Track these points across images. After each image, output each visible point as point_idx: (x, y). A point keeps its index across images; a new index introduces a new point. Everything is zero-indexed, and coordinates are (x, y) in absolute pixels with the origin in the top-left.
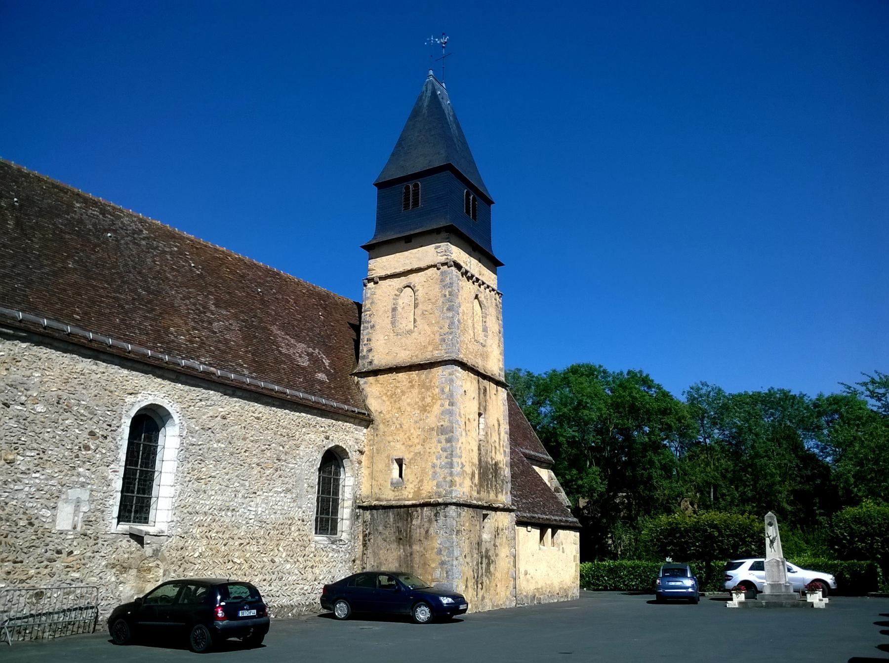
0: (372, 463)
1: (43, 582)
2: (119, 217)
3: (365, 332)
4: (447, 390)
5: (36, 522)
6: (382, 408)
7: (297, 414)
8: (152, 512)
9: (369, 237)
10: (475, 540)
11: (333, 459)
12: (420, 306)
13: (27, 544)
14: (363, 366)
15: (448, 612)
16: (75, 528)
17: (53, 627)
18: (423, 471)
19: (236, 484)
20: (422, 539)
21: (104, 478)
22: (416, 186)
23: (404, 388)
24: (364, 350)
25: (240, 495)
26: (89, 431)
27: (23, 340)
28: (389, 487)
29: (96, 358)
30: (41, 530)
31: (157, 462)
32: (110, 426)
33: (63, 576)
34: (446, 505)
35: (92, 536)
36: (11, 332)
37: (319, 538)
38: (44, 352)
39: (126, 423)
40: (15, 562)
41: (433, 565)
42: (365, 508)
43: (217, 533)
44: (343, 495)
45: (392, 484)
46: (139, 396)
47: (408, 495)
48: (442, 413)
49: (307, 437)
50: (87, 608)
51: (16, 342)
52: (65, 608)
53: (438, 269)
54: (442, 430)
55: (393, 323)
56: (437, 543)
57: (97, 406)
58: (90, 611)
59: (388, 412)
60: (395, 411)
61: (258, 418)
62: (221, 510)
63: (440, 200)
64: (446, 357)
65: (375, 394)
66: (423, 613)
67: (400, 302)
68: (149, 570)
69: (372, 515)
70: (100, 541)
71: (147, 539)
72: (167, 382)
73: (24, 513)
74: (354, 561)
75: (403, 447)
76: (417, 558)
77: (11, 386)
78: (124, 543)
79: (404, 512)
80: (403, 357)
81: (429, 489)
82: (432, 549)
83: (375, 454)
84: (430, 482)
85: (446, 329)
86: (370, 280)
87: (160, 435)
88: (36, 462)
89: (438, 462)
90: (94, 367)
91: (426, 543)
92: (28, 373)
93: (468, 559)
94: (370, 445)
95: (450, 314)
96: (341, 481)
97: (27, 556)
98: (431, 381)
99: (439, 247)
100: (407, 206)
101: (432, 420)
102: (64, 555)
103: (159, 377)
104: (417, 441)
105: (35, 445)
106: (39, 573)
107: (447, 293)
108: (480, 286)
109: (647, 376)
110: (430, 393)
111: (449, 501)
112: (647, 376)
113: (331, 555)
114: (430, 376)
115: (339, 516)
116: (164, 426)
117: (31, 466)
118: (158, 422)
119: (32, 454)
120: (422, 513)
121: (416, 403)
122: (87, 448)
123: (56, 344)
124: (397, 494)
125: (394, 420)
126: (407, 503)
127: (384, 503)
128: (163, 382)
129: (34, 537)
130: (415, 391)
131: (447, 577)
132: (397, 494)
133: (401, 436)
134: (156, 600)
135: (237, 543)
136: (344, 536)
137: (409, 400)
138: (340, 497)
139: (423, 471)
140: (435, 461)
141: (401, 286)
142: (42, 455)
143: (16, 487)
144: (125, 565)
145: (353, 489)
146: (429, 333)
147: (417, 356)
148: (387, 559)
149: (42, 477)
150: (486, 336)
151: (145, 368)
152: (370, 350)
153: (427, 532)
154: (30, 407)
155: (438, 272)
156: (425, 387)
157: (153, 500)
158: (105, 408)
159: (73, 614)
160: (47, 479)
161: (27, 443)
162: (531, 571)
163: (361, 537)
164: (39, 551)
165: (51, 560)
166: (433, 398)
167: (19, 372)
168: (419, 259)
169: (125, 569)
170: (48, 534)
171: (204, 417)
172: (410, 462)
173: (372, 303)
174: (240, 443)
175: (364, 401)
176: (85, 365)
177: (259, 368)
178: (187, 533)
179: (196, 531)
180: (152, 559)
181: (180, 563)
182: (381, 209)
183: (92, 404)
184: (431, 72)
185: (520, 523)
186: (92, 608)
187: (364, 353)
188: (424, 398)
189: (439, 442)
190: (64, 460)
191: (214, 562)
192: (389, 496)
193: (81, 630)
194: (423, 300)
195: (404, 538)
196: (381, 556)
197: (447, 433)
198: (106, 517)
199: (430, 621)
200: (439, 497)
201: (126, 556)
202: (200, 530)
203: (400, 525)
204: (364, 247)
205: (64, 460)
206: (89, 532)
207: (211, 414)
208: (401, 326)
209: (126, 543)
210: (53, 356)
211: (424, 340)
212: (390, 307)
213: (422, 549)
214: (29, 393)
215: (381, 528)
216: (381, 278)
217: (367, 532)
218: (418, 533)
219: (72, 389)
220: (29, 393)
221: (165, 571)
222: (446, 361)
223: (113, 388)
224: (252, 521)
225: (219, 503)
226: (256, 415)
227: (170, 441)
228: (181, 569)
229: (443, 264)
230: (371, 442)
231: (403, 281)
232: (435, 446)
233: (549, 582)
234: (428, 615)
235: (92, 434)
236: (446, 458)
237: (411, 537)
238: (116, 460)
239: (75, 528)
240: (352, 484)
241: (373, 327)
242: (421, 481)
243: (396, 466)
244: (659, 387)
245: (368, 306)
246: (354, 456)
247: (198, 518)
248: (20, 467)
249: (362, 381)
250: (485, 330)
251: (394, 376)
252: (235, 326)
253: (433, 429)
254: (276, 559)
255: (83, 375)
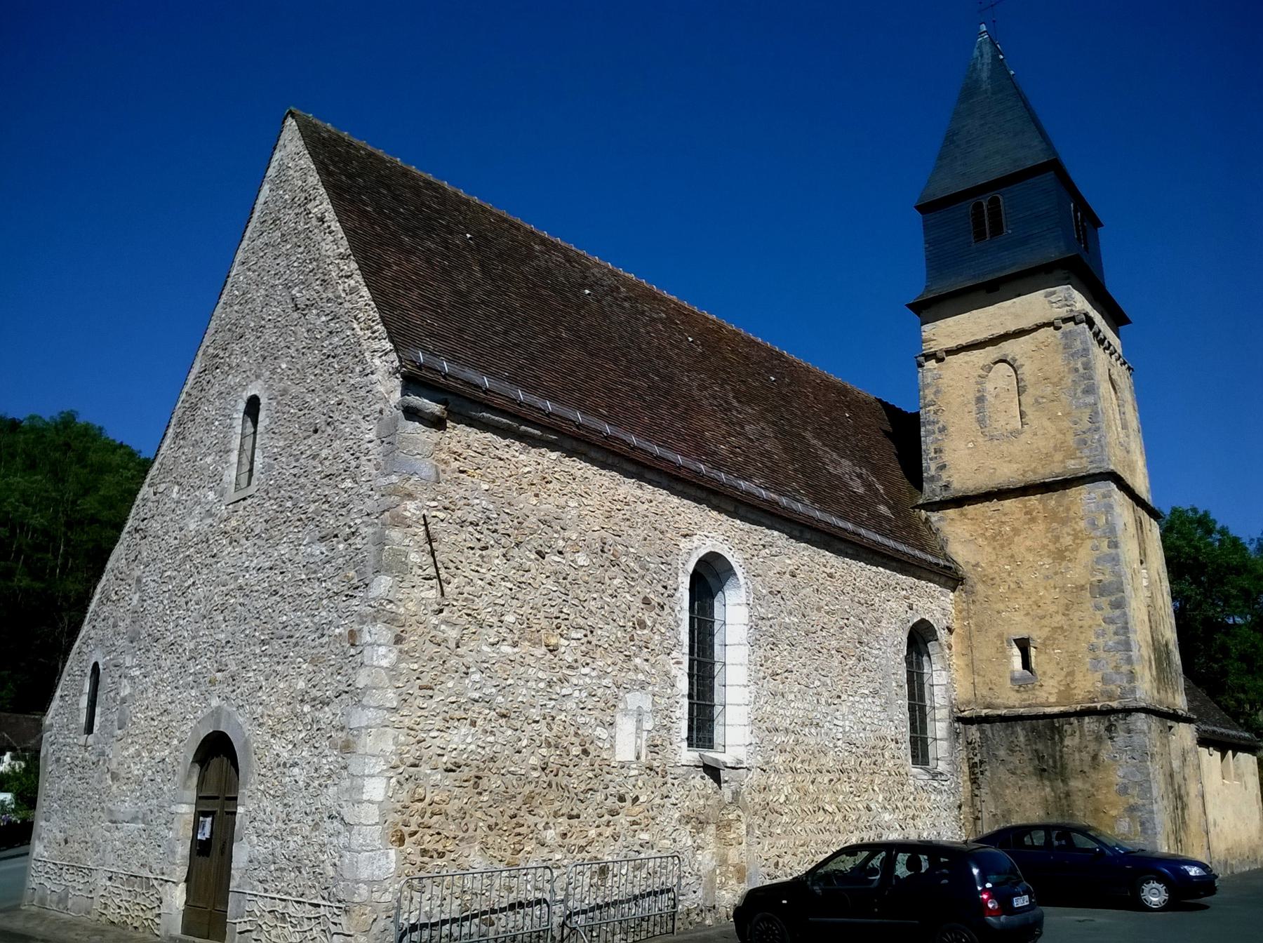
0: (971, 647)
1: (607, 850)
2: (588, 268)
3: (930, 439)
4: (1102, 521)
5: (591, 749)
6: (979, 558)
7: (874, 568)
8: (718, 731)
9: (917, 291)
10: (1167, 768)
11: (920, 638)
12: (1030, 390)
13: (583, 787)
14: (931, 491)
15: (1191, 889)
16: (638, 758)
17: (624, 925)
18: (1073, 657)
19: (817, 683)
20: (1086, 769)
21: (667, 674)
22: (994, 202)
23: (1017, 524)
24: (930, 466)
25: (823, 701)
26: (642, 596)
27: (552, 446)
28: (1009, 684)
29: (640, 478)
30: (598, 761)
31: (716, 647)
32: (665, 587)
33: (629, 839)
34: (1128, 711)
35: (659, 770)
36: (538, 433)
37: (915, 771)
38: (578, 467)
39: (685, 582)
40: (571, 817)
41: (1114, 813)
42: (967, 721)
43: (802, 762)
44: (932, 701)
45: (1013, 680)
46: (695, 538)
47: (1047, 696)
48: (1098, 561)
49: (887, 606)
50: (662, 892)
51: (543, 450)
52: (637, 892)
53: (1057, 328)
54: (1101, 589)
55: (981, 422)
56: (1117, 775)
57: (649, 555)
58: (665, 896)
59: (991, 564)
60: (1003, 561)
61: (831, 576)
62: (803, 724)
63: (1006, 228)
64: (1093, 469)
65: (960, 536)
66: (1155, 895)
67: (989, 386)
68: (729, 825)
69: (983, 732)
70: (669, 779)
71: (725, 775)
72: (724, 517)
73: (576, 734)
74: (960, 807)
75: (1027, 620)
76: (1079, 802)
77: (544, 522)
78: (697, 782)
79: (1046, 726)
80: (1007, 473)
81: (1087, 686)
82: (1109, 785)
83: (975, 633)
84: (1089, 677)
85: (1086, 424)
86: (928, 357)
87: (716, 604)
88: (583, 648)
89: (1101, 642)
90: (639, 492)
91: (1094, 776)
92: (562, 501)
93: (1165, 802)
94: (963, 619)
95: (1090, 399)
96: (926, 678)
97: (584, 806)
98: (1068, 509)
99: (1054, 293)
100: (980, 235)
101: (1078, 572)
102: (628, 803)
103: (714, 509)
104: (1053, 608)
105: (581, 621)
106: (600, 834)
107: (1079, 366)
108: (1111, 354)
109: (1206, 514)
110: (1069, 530)
111: (1133, 705)
112: (1206, 514)
113: (933, 797)
114: (1066, 501)
115: (929, 734)
116: (721, 588)
117: (579, 656)
118: (711, 580)
119: (579, 636)
120: (1081, 726)
121: (1044, 547)
122: (642, 625)
123: (593, 454)
124: (1025, 696)
125: (1004, 575)
126: (1048, 710)
127: (1003, 712)
128: (719, 517)
129: (590, 774)
130: (1040, 527)
131: (1144, 831)
132: (1025, 696)
133: (1021, 602)
134: (829, 876)
135: (826, 780)
136: (942, 766)
137: (1028, 543)
138: (928, 702)
139: (1073, 657)
140: (1094, 640)
141: (988, 361)
142: (590, 637)
143: (564, 692)
144: (702, 817)
145: (947, 690)
146: (1053, 432)
147: (1034, 471)
148: (1027, 804)
149: (594, 674)
150: (1128, 436)
151: (699, 494)
152: (943, 467)
153: (1095, 757)
154: (568, 555)
155: (1058, 333)
156: (1052, 517)
157: (717, 710)
158: (659, 560)
159: (646, 903)
160: (599, 677)
161: (571, 618)
162: (1219, 821)
163: (966, 769)
164: (599, 797)
165: (614, 813)
166: (1076, 537)
167: (551, 500)
168: (1017, 316)
169: (701, 824)
170: (606, 769)
171: (771, 574)
172: (1044, 644)
173: (937, 392)
174: (814, 616)
175: (942, 548)
176: (628, 488)
177: (818, 498)
178: (767, 763)
179: (778, 759)
180: (731, 808)
181: (764, 812)
182: (932, 243)
183: (642, 552)
184: (983, 27)
185: (1204, 741)
186: (668, 891)
187: (932, 472)
188: (1057, 538)
189: (1098, 608)
190: (617, 644)
191: (803, 810)
192: (1010, 700)
193: (657, 929)
194: (1033, 380)
195: (1050, 768)
196: (1008, 798)
197: (1111, 594)
198: (674, 739)
199: (1168, 907)
200: (1111, 698)
201: (701, 802)
202: (782, 758)
203: (1040, 746)
204: (910, 306)
205: (617, 644)
206: (655, 764)
207: (778, 569)
208: (995, 425)
209: (701, 782)
210: (589, 474)
211: (1042, 444)
212: (971, 397)
213: (1088, 786)
214: (567, 534)
215: (1002, 753)
216: (950, 352)
217: (976, 760)
218: (1076, 760)
219: (617, 528)
220: (567, 534)
221: (748, 826)
222: (1094, 475)
223: (664, 527)
224: (839, 743)
225: (801, 713)
226: (828, 570)
227: (733, 611)
228: (766, 824)
229: (1065, 320)
230: (964, 614)
231: (992, 353)
232: (1090, 615)
233: (1237, 838)
234: (1165, 896)
235: (646, 601)
236: (1116, 633)
237: (1063, 767)
238: (678, 644)
239: (638, 758)
240: (945, 681)
241: (943, 429)
242: (1071, 674)
243: (1016, 651)
244: (1223, 532)
245: (930, 397)
246: (942, 635)
247: (779, 738)
248: (566, 656)
249: (934, 517)
250: (1124, 427)
251: (995, 504)
252: (769, 432)
253: (1082, 588)
254: (873, 806)
255: (627, 504)
